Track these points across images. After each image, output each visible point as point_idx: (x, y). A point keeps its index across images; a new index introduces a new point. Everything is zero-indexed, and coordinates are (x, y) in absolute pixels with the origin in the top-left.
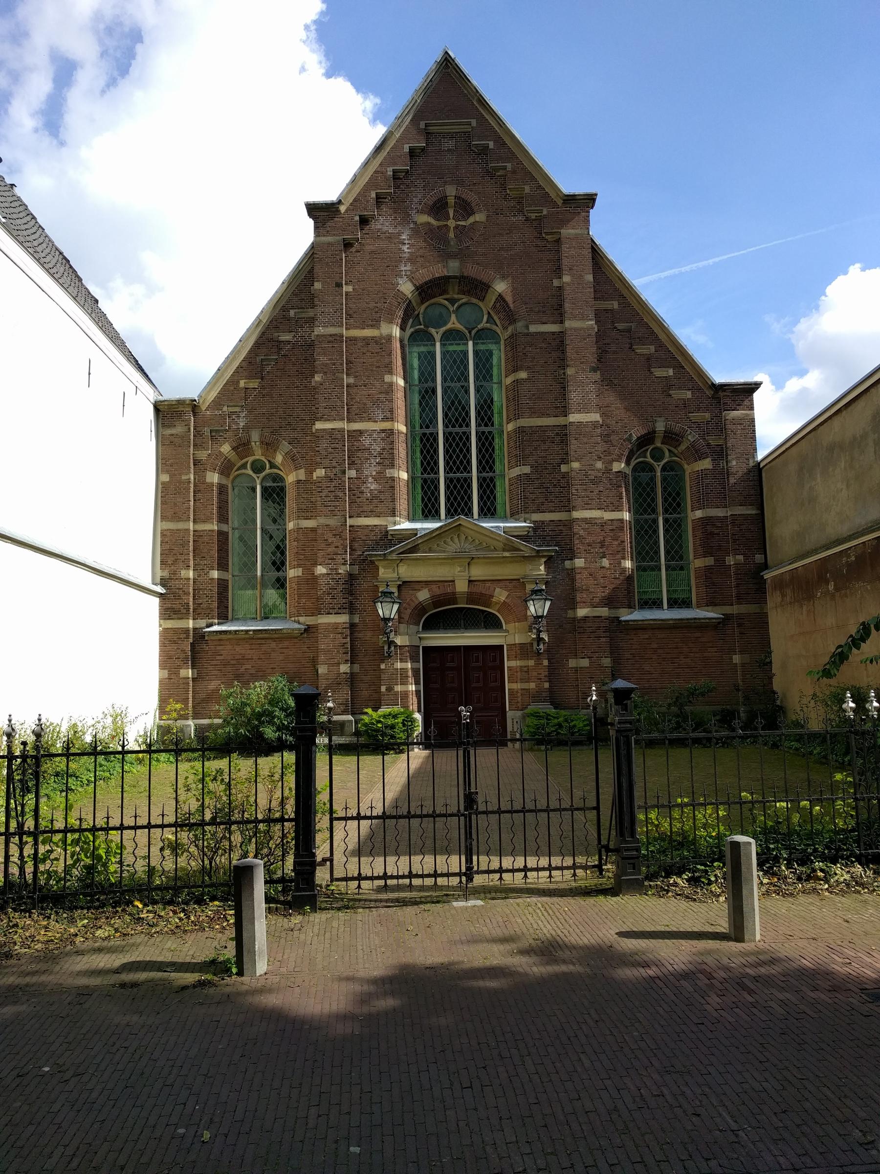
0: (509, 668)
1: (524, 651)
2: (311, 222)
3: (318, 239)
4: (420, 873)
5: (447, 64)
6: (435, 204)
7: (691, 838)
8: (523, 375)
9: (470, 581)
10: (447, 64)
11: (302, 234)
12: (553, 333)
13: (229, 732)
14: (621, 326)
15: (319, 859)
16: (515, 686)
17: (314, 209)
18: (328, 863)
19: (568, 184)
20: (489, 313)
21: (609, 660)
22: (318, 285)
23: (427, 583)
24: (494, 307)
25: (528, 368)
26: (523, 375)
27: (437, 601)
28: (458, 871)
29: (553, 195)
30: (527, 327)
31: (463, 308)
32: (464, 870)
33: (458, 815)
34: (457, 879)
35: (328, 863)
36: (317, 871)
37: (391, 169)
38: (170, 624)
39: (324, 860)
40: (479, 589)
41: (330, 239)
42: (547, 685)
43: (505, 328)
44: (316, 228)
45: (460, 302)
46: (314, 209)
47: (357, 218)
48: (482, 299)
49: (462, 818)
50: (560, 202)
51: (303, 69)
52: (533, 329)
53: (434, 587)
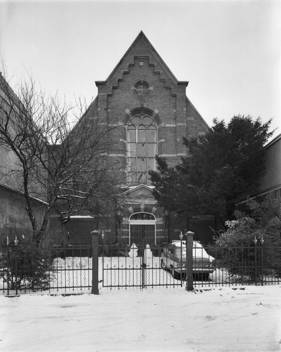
1: (159, 226)
3: (100, 94)
4: (129, 285)
5: (141, 37)
8: (163, 140)
10: (141, 37)
11: (93, 93)
12: (173, 127)
15: (99, 281)
17: (98, 84)
18: (102, 282)
20: (153, 120)
22: (99, 109)
25: (165, 139)
26: (163, 140)
29: (175, 82)
32: (141, 285)
33: (140, 269)
34: (267, 280)
35: (102, 282)
36: (87, 258)
37: (122, 71)
38: (81, 256)
39: (101, 281)
41: (103, 94)
42: (168, 237)
43: (158, 125)
44: (98, 90)
46: (98, 84)
47: (112, 87)
48: (151, 116)
49: (141, 270)
50: (176, 84)
51: (100, 289)
52: (167, 125)
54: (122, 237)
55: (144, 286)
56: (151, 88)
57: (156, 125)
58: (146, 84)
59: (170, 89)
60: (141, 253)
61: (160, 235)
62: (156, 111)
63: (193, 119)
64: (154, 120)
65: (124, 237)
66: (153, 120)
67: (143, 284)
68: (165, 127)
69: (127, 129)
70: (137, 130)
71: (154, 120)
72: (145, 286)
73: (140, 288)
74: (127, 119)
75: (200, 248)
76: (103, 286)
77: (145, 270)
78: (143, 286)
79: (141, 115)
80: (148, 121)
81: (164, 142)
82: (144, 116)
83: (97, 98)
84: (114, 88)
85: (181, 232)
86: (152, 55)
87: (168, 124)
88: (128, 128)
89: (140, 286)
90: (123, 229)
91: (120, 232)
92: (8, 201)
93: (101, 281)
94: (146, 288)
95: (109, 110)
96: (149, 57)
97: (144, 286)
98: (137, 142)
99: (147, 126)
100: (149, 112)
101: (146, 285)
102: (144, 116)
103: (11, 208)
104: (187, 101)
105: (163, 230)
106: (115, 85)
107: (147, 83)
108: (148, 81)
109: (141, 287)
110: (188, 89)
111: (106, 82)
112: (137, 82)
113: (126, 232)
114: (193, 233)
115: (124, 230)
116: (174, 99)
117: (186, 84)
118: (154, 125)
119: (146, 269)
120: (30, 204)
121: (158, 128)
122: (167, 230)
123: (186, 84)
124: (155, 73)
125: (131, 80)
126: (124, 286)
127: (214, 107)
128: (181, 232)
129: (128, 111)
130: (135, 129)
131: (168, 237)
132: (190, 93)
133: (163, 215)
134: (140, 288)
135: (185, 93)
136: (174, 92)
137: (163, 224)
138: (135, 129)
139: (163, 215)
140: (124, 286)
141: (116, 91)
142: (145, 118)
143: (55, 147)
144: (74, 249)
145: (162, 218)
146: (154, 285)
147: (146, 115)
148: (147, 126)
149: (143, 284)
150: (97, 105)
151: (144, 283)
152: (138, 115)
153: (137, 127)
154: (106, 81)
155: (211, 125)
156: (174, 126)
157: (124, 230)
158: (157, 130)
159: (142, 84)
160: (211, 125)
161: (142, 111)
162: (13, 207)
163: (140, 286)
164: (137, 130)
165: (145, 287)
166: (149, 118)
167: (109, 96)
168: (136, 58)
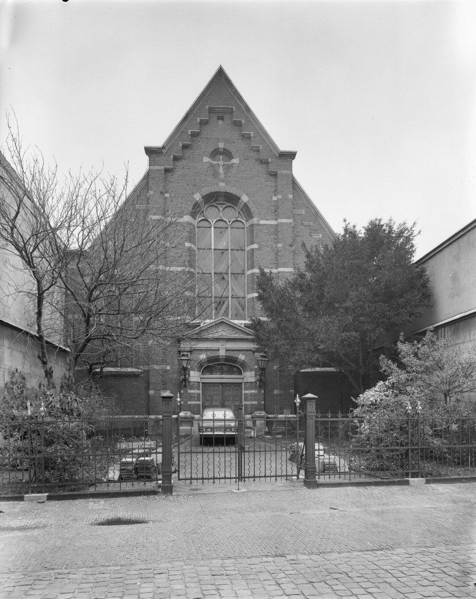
0: (245, 394)
2: (147, 158)
4: (218, 477)
5: (220, 77)
6: (213, 152)
7: (404, 348)
8: (255, 246)
9: (226, 350)
10: (220, 77)
11: (141, 166)
12: (272, 225)
13: (413, 356)
14: (306, 223)
16: (246, 403)
18: (177, 472)
19: (283, 146)
20: (239, 212)
21: (293, 391)
23: (206, 350)
24: (242, 210)
26: (255, 246)
27: (210, 360)
28: (234, 476)
30: (259, 221)
31: (228, 208)
35: (177, 472)
40: (231, 354)
42: (263, 403)
43: (247, 221)
45: (242, 220)
46: (149, 151)
48: (236, 206)
49: (237, 453)
53: (209, 353)
54: (189, 403)
55: (242, 478)
56: (235, 161)
57: (243, 221)
58: (227, 154)
59: (267, 163)
60: (219, 428)
61: (251, 400)
62: (245, 198)
63: (304, 213)
64: (241, 212)
65: (193, 403)
66: (239, 212)
67: (240, 474)
68: (258, 225)
69: (196, 226)
70: (213, 228)
71: (241, 212)
72: (243, 477)
73: (236, 481)
74: (196, 210)
75: (233, 420)
76: (179, 479)
77: (243, 453)
78: (240, 478)
79: (219, 204)
80: (230, 214)
81: (256, 249)
82: (224, 206)
83: (147, 176)
84: (176, 159)
85: (298, 396)
86: (238, 107)
87: (263, 219)
88: (199, 226)
89: (236, 478)
90: (191, 389)
91: (185, 395)
92: (6, 343)
93: (175, 472)
94: (244, 481)
95: (167, 195)
96: (232, 109)
97: (242, 478)
98: (213, 247)
99: (229, 222)
100: (231, 199)
101: (244, 478)
102: (224, 206)
103: (11, 355)
104: (294, 184)
105: (256, 391)
106: (179, 154)
107: (229, 151)
108: (232, 149)
109: (237, 479)
110: (295, 162)
111: (163, 147)
112: (213, 149)
113: (196, 395)
114: (315, 396)
115: (192, 391)
116: (272, 179)
117: (292, 155)
118: (240, 221)
119: (244, 452)
120: (40, 346)
121: (247, 225)
122: (263, 391)
123: (292, 155)
124: (243, 136)
125: (204, 147)
126: (211, 479)
127: (344, 204)
128: (298, 396)
129: (198, 197)
130: (209, 226)
131: (152, 392)
132: (299, 170)
133: (256, 367)
134: (236, 481)
135: (291, 170)
136: (272, 168)
137: (256, 382)
138: (210, 227)
139: (256, 367)
140: (211, 479)
141: (180, 163)
142: (226, 210)
143: (80, 254)
144: (331, 421)
145: (253, 373)
146: (257, 477)
147: (229, 204)
148: (229, 222)
149: (239, 475)
150: (147, 184)
151: (241, 473)
152: (214, 204)
153: (213, 223)
154: (163, 146)
155: (338, 229)
156: (273, 222)
157: (192, 391)
158: (246, 228)
159: (221, 154)
160: (338, 229)
161: (221, 198)
162: (13, 354)
163: (236, 478)
164: (213, 228)
165: (243, 479)
166: (233, 210)
167: (167, 171)
168: (211, 111)
